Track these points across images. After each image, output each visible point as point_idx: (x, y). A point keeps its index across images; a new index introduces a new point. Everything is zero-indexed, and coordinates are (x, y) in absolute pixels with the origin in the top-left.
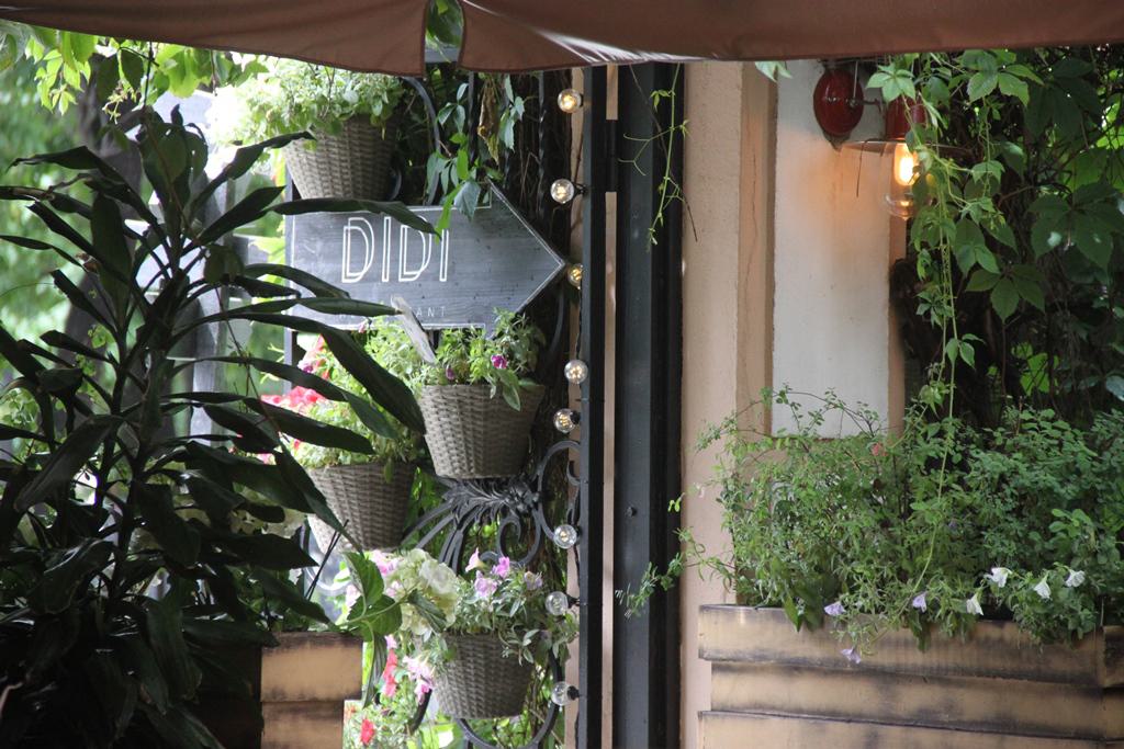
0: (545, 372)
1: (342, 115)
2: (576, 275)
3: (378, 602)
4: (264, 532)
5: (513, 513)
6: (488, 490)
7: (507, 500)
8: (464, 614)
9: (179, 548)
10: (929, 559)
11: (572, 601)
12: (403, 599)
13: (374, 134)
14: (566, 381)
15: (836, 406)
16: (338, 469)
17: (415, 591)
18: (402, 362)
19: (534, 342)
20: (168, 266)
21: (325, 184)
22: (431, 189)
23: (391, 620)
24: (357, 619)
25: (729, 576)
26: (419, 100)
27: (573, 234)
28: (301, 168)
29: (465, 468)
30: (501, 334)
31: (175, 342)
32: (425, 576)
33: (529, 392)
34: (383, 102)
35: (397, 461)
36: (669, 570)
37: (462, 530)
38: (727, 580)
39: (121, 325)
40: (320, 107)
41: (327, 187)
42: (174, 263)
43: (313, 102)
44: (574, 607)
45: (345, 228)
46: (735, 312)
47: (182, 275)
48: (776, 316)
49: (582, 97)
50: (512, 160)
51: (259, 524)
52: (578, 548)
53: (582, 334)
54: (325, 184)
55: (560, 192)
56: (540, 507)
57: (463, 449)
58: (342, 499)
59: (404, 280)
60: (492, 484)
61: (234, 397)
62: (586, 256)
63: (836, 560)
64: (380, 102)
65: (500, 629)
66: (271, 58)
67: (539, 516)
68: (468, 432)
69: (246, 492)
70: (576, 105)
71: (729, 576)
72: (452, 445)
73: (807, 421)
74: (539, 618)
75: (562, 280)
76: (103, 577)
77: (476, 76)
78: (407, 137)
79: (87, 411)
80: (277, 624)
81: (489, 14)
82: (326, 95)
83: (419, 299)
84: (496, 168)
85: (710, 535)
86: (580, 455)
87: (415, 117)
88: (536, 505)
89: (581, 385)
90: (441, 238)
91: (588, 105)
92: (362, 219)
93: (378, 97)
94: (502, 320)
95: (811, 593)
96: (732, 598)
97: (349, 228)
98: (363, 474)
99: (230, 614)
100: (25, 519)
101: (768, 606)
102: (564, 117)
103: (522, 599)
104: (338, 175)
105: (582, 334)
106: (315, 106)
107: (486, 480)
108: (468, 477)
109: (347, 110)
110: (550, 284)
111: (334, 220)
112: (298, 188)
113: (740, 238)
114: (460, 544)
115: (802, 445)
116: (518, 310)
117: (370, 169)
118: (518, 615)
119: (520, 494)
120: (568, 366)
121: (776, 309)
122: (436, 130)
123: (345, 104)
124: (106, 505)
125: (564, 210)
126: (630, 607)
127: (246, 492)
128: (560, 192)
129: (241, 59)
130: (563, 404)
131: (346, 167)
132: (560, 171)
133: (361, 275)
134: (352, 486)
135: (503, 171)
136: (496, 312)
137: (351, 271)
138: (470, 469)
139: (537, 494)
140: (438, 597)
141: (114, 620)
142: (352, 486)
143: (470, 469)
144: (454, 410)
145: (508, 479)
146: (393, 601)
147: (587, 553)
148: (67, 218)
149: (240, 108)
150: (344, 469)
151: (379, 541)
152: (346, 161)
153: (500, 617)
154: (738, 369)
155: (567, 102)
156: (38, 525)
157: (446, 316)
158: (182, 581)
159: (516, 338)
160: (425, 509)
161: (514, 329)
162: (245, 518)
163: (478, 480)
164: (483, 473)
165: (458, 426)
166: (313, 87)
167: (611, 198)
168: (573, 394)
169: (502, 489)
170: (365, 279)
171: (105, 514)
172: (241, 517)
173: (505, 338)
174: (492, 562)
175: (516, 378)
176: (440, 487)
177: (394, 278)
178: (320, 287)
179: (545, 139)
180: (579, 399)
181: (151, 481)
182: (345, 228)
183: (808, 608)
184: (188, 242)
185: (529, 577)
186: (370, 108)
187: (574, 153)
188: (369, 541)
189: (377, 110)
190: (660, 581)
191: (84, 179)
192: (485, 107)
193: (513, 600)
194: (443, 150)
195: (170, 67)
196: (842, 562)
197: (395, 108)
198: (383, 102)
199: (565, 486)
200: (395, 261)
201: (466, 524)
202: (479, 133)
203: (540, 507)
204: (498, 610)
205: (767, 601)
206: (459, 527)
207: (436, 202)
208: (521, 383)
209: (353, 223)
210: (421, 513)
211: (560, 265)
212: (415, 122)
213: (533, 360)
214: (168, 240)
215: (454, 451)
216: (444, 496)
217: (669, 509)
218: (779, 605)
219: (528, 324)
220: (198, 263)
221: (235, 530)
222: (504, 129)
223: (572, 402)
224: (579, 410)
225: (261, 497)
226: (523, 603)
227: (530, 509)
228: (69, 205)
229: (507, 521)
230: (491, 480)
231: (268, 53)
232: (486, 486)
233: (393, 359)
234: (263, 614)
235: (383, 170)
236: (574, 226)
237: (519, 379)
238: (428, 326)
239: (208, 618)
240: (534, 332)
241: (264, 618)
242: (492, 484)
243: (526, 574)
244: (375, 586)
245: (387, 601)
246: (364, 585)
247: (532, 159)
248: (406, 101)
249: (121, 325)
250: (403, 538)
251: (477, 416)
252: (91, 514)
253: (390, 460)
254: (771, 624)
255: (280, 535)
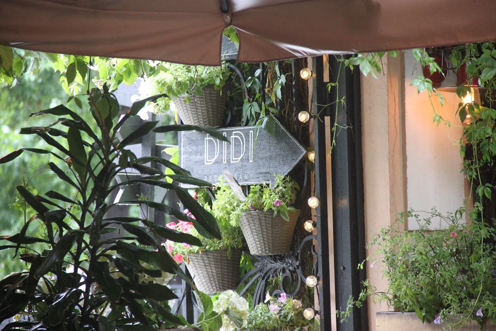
0: (300, 202)
1: (201, 86)
2: (312, 156)
3: (210, 314)
4: (154, 282)
5: (288, 271)
6: (275, 260)
7: (285, 265)
8: (265, 320)
9: (113, 291)
10: (481, 288)
11: (316, 313)
12: (222, 313)
13: (216, 94)
14: (310, 208)
15: (437, 215)
16: (205, 253)
17: (228, 308)
18: (232, 201)
19: (294, 189)
20: (104, 159)
21: (195, 118)
22: (244, 119)
23: (217, 324)
24: (201, 322)
25: (390, 300)
26: (238, 76)
27: (311, 137)
28: (183, 111)
29: (263, 250)
30: (278, 186)
31: (109, 193)
32: (233, 301)
33: (292, 213)
34: (220, 79)
35: (233, 249)
36: (360, 298)
37: (264, 280)
38: (389, 302)
39: (83, 187)
40: (190, 82)
41: (196, 120)
42: (106, 157)
43: (188, 80)
44: (317, 315)
45: (231, 137)
46: (388, 171)
47: (110, 162)
48: (408, 172)
49: (311, 71)
50: (281, 104)
51: (151, 279)
52: (318, 287)
53: (316, 184)
54: (195, 118)
55: (303, 117)
56: (300, 267)
57: (262, 241)
58: (207, 267)
59: (234, 162)
60: (277, 257)
61: (137, 219)
62: (317, 148)
63: (439, 289)
64: (219, 79)
65: (283, 327)
66: (167, 63)
67: (299, 271)
68: (264, 233)
69: (144, 265)
70: (309, 76)
71: (390, 300)
72: (257, 240)
73: (423, 223)
74: (301, 321)
75: (305, 159)
76: (79, 306)
77: (263, 64)
78: (233, 94)
79: (68, 227)
80: (163, 325)
81: (248, 34)
82: (193, 77)
83: (233, 174)
84: (274, 107)
85: (380, 280)
86: (317, 243)
87: (237, 84)
88: (298, 266)
89: (316, 208)
90: (230, 143)
91: (314, 75)
92: (240, 132)
93: (217, 76)
94: (279, 179)
95: (430, 306)
96: (392, 309)
97: (207, 138)
98: (216, 255)
99: (141, 322)
100: (41, 279)
101: (408, 312)
102: (304, 82)
103: (292, 313)
104: (200, 113)
105: (316, 184)
106: (188, 82)
107: (275, 256)
108: (265, 255)
109: (203, 83)
110: (300, 161)
111: (200, 135)
112: (183, 121)
113: (389, 136)
114: (264, 286)
115: (423, 232)
116: (286, 174)
117: (215, 110)
118: (291, 320)
119: (290, 262)
120: (309, 200)
121: (408, 169)
122: (246, 90)
123: (202, 80)
124: (80, 271)
125: (306, 125)
126: (342, 318)
127: (144, 265)
128: (303, 117)
129: (152, 64)
130: (309, 218)
131: (204, 110)
132: (304, 107)
133: (213, 160)
134: (212, 261)
135: (277, 108)
136: (275, 175)
137: (209, 159)
138: (266, 250)
139: (298, 262)
140: (238, 312)
141: (85, 326)
142: (212, 261)
143: (266, 250)
144: (257, 223)
145: (285, 255)
146: (217, 314)
147: (322, 289)
148: (55, 138)
149: (150, 86)
150: (207, 253)
151: (226, 287)
152: (204, 107)
153: (282, 321)
154: (390, 199)
155: (305, 74)
156: (47, 282)
157: (253, 178)
158: (117, 307)
159: (285, 187)
160: (247, 271)
161: (284, 183)
162: (145, 276)
163: (271, 256)
164: (272, 252)
165: (259, 230)
166: (187, 73)
167: (327, 119)
168: (314, 213)
169: (282, 260)
170: (216, 162)
171: (80, 277)
172: (143, 276)
173: (280, 188)
174: (277, 296)
175: (286, 206)
176: (254, 259)
177: (228, 162)
178: (175, 168)
179: (296, 94)
180: (316, 216)
181: (99, 260)
182: (205, 139)
183: (426, 312)
184: (112, 148)
185: (295, 302)
186: (215, 82)
187: (310, 98)
188: (221, 287)
189: (218, 82)
190: (355, 304)
191: (61, 122)
192: (269, 80)
193: (288, 313)
194: (79, 103)
195: (123, 71)
196: (441, 289)
197: (227, 81)
198: (220, 79)
199: (311, 256)
200: (229, 154)
201: (266, 278)
202: (266, 92)
203: (300, 267)
204: (281, 318)
205: (407, 310)
206: (263, 279)
207: (247, 125)
208: (288, 209)
209: (235, 134)
210: (246, 272)
211: (305, 152)
212: (236, 87)
213: (294, 198)
214: (104, 146)
215: (258, 243)
216: (256, 264)
217: (358, 268)
218: (413, 311)
219: (291, 180)
220: (116, 158)
221: (140, 282)
222: (313, 90)
223: (313, 217)
224: (316, 221)
225: (152, 266)
226: (293, 314)
227: (295, 269)
228: (58, 133)
229: (285, 275)
230: (277, 255)
231: (166, 61)
232: (275, 258)
233: (227, 200)
234: (156, 321)
235: (222, 110)
236: (311, 133)
237: (288, 207)
238: (241, 184)
239: (131, 324)
240: (294, 185)
241: (156, 323)
242: (277, 257)
243: (294, 301)
244: (209, 306)
245: (214, 314)
246: (204, 306)
247: (290, 102)
248: (232, 77)
249: (83, 187)
250: (238, 285)
251: (268, 225)
252: (72, 277)
253: (229, 248)
254: (410, 320)
255: (161, 284)
